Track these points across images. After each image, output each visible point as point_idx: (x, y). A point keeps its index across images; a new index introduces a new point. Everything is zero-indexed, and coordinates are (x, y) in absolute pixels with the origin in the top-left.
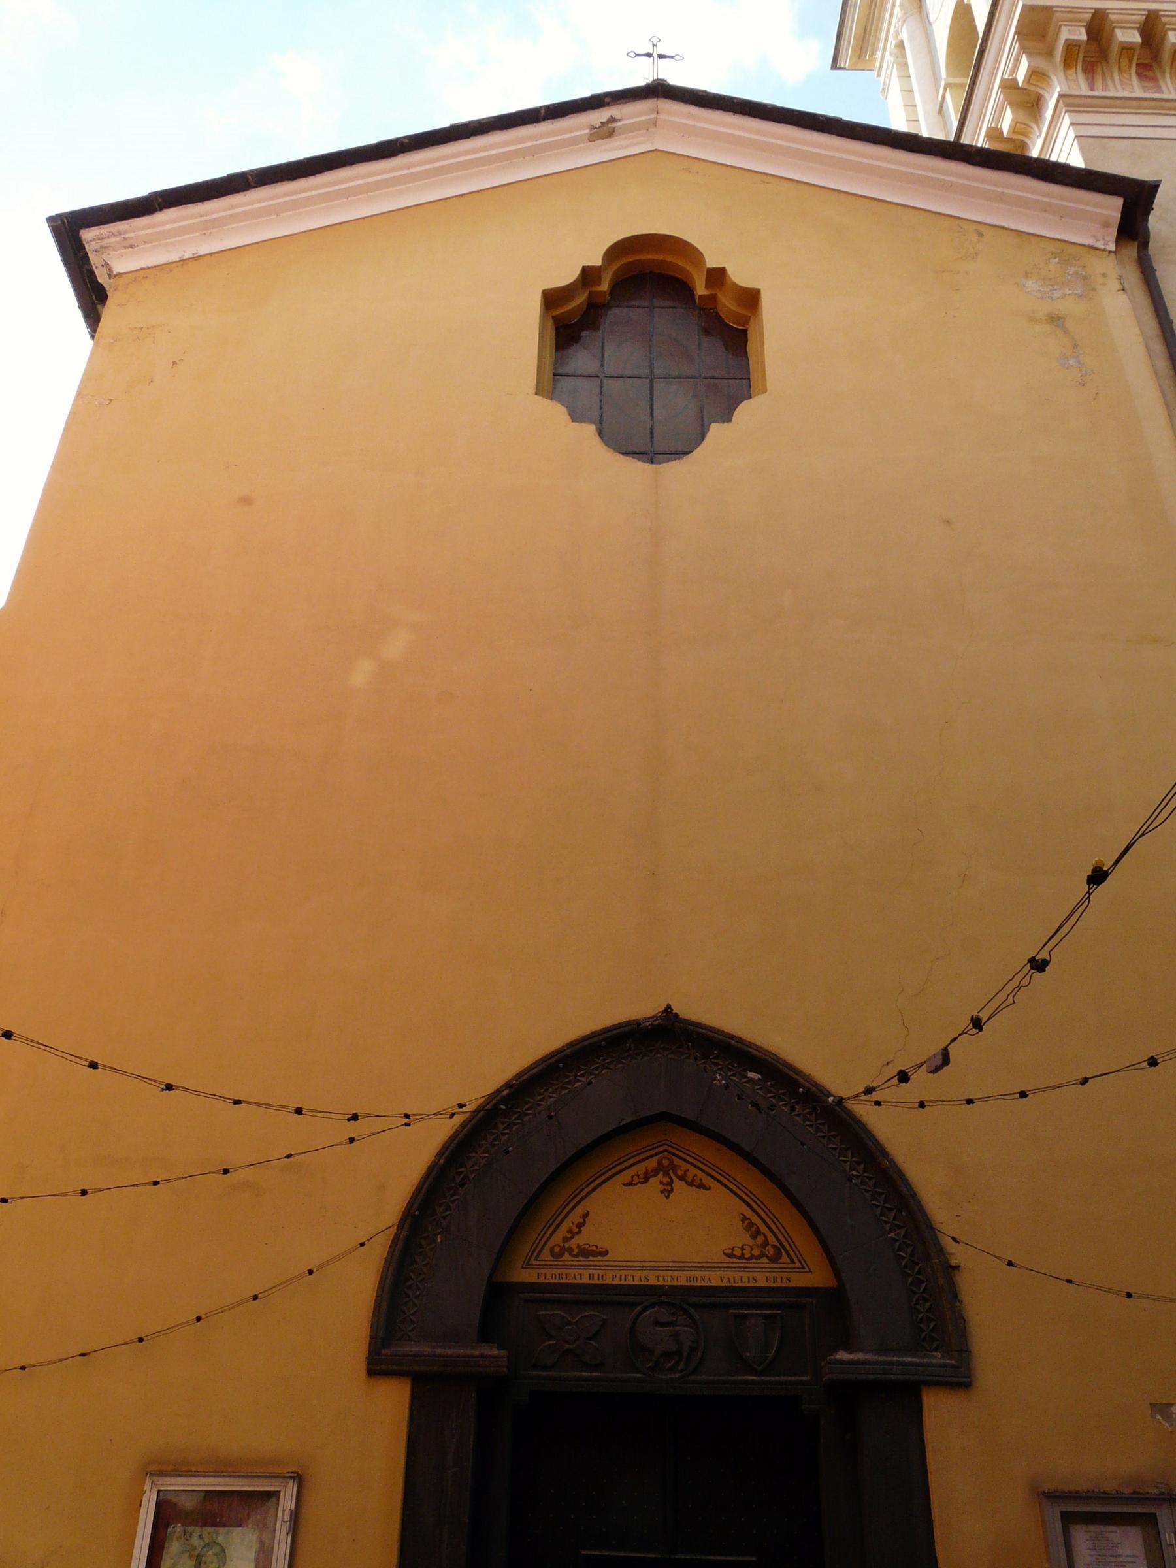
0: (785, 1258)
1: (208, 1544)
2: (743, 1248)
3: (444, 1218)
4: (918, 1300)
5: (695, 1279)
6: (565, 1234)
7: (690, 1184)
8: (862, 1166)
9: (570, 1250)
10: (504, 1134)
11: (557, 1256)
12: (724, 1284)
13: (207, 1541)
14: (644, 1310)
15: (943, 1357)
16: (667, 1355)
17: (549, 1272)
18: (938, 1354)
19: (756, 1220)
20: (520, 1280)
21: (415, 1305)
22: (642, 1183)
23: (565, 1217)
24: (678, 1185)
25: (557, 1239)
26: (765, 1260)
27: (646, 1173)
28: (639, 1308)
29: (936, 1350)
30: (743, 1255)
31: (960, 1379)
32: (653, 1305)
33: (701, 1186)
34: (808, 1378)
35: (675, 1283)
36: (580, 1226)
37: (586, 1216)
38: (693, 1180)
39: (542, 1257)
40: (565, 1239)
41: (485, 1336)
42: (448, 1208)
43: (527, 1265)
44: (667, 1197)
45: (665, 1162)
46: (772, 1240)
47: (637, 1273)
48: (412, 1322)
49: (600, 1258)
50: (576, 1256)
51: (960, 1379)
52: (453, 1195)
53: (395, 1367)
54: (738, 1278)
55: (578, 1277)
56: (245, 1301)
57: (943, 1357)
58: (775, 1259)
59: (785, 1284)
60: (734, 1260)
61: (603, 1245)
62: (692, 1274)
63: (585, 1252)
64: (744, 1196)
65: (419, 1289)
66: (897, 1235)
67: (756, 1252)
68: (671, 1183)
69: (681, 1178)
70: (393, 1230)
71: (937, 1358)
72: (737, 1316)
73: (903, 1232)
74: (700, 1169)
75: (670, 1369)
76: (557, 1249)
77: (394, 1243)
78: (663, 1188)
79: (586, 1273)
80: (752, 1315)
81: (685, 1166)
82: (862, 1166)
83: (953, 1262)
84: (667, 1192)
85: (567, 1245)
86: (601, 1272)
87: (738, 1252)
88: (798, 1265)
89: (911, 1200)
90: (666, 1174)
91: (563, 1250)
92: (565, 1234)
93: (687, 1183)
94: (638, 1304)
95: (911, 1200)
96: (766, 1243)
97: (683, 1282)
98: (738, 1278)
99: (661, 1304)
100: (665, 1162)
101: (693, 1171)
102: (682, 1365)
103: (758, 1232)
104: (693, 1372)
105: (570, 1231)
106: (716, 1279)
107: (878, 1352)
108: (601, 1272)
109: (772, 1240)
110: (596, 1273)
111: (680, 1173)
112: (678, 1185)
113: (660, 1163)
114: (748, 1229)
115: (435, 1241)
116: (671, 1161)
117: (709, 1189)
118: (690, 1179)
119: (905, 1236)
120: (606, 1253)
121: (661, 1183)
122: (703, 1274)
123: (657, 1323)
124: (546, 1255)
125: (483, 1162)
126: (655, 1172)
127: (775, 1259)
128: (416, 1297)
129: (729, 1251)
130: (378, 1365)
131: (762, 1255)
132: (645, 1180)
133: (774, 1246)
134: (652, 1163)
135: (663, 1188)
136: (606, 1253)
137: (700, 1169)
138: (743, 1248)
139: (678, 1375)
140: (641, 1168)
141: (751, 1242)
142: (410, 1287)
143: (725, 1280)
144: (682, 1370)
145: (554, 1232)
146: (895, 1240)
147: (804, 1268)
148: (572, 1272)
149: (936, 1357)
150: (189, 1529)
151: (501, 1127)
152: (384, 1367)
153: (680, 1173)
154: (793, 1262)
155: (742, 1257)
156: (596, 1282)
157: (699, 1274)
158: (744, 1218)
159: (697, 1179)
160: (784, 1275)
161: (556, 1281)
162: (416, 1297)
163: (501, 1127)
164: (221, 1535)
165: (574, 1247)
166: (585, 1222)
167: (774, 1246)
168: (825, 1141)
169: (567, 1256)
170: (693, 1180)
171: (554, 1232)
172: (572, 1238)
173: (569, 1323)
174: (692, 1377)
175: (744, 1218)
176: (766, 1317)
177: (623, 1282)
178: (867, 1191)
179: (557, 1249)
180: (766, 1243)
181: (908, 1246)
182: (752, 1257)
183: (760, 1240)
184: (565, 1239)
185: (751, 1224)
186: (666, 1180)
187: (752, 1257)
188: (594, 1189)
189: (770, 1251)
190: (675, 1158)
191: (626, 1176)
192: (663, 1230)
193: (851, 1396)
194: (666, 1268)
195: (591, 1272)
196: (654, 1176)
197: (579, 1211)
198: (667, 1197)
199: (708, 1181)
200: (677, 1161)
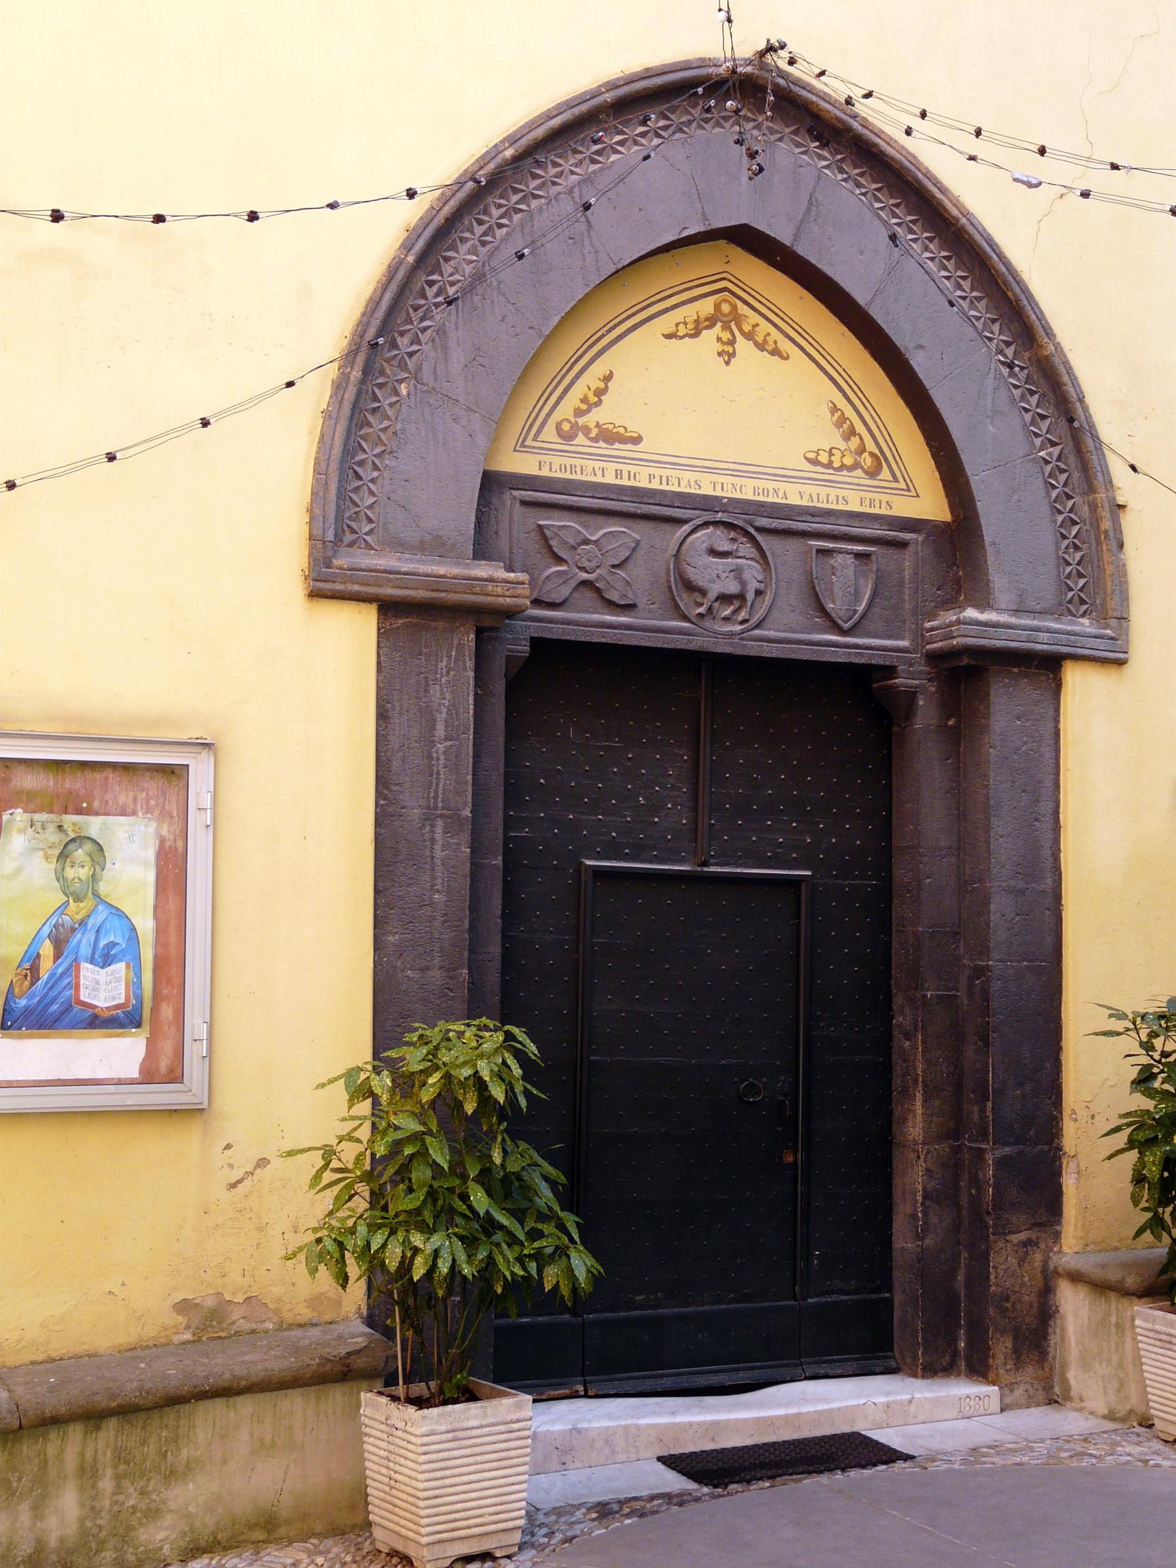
0: (885, 473)
1: (73, 840)
2: (831, 454)
3: (411, 355)
4: (1067, 548)
5: (766, 492)
6: (578, 404)
7: (761, 347)
8: (1012, 348)
9: (586, 430)
10: (500, 226)
11: (567, 437)
12: (804, 503)
13: (72, 835)
14: (693, 531)
15: (1091, 625)
16: (725, 598)
17: (557, 461)
18: (1085, 621)
19: (849, 412)
20: (496, 469)
21: (372, 493)
22: (692, 336)
23: (577, 376)
24: (743, 346)
25: (566, 410)
26: (859, 473)
27: (697, 322)
28: (686, 528)
29: (1083, 615)
30: (831, 462)
31: (1113, 659)
32: (706, 524)
33: (775, 352)
34: (904, 643)
35: (738, 495)
36: (599, 393)
37: (608, 378)
38: (765, 341)
39: (542, 437)
40: (579, 413)
41: (481, 551)
42: (416, 341)
43: (521, 446)
44: (727, 363)
45: (726, 308)
46: (870, 446)
47: (687, 476)
48: (370, 520)
49: (630, 446)
50: (595, 440)
51: (1113, 659)
52: (422, 319)
53: (357, 588)
54: (823, 497)
55: (599, 473)
56: (89, 463)
57: (1091, 625)
58: (873, 473)
59: (884, 511)
60: (819, 469)
61: (634, 427)
62: (762, 484)
63: (609, 436)
64: (835, 375)
65: (376, 468)
66: (1050, 454)
67: (848, 461)
68: (732, 342)
69: (749, 336)
70: (333, 371)
71: (1085, 625)
72: (821, 552)
73: (1056, 451)
74: (776, 326)
75: (726, 619)
76: (566, 427)
77: (339, 387)
78: (720, 348)
79: (611, 467)
80: (840, 551)
81: (754, 318)
82: (1012, 348)
83: (1120, 500)
84: (728, 356)
85: (581, 421)
86: (633, 469)
87: (824, 458)
88: (902, 485)
89: (1078, 405)
90: (726, 327)
91: (575, 427)
92: (578, 404)
93: (757, 344)
94: (682, 522)
95: (1078, 405)
96: (862, 450)
97: (748, 495)
98: (823, 497)
99: (716, 523)
100: (726, 308)
101: (765, 327)
102: (743, 615)
103: (852, 432)
104: (757, 627)
105: (584, 400)
106: (794, 495)
107: (1016, 612)
108: (633, 469)
109: (870, 446)
110: (625, 468)
111: (747, 328)
112: (743, 346)
113: (717, 307)
114: (839, 424)
115: (396, 392)
116: (734, 307)
117: (787, 358)
118: (760, 339)
119: (1059, 459)
120: (637, 440)
121: (719, 339)
122: (776, 485)
123: (713, 552)
124: (549, 433)
125: (468, 269)
126: (711, 322)
127: (873, 473)
128: (373, 481)
129: (812, 456)
130: (325, 587)
131: (856, 466)
132: (696, 334)
133: (872, 454)
134: (706, 307)
135: (720, 348)
136: (637, 440)
137: (776, 326)
138: (831, 454)
139: (739, 628)
140: (688, 312)
141: (842, 445)
142: (361, 463)
143: (806, 497)
144: (745, 621)
145: (560, 398)
146: (1047, 462)
147: (909, 489)
148: (590, 464)
149: (1083, 625)
150: (37, 817)
151: (496, 213)
152: (338, 587)
153: (747, 328)
154: (896, 480)
155: (829, 465)
156: (625, 482)
157: (770, 485)
158: (834, 409)
159: (770, 340)
160: (885, 498)
161: (568, 476)
162: (373, 481)
163: (496, 213)
164: (94, 825)
165: (592, 425)
166: (607, 388)
167: (872, 454)
168: (965, 304)
169: (581, 439)
170: (765, 341)
171: (560, 398)
172: (588, 411)
173: (586, 542)
174: (757, 632)
175: (834, 409)
176: (858, 556)
177: (664, 487)
178: (1016, 387)
179: (566, 427)
180: (862, 450)
181: (1063, 471)
182: (843, 467)
183: (854, 442)
184: (579, 413)
185: (843, 419)
186: (726, 336)
187: (843, 467)
188: (620, 337)
189: (867, 461)
190: (739, 304)
191: (666, 323)
192: (722, 417)
193: (966, 673)
194: (735, 473)
195: (620, 467)
196: (707, 328)
197: (599, 369)
198: (727, 363)
199: (785, 346)
200: (743, 309)
